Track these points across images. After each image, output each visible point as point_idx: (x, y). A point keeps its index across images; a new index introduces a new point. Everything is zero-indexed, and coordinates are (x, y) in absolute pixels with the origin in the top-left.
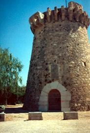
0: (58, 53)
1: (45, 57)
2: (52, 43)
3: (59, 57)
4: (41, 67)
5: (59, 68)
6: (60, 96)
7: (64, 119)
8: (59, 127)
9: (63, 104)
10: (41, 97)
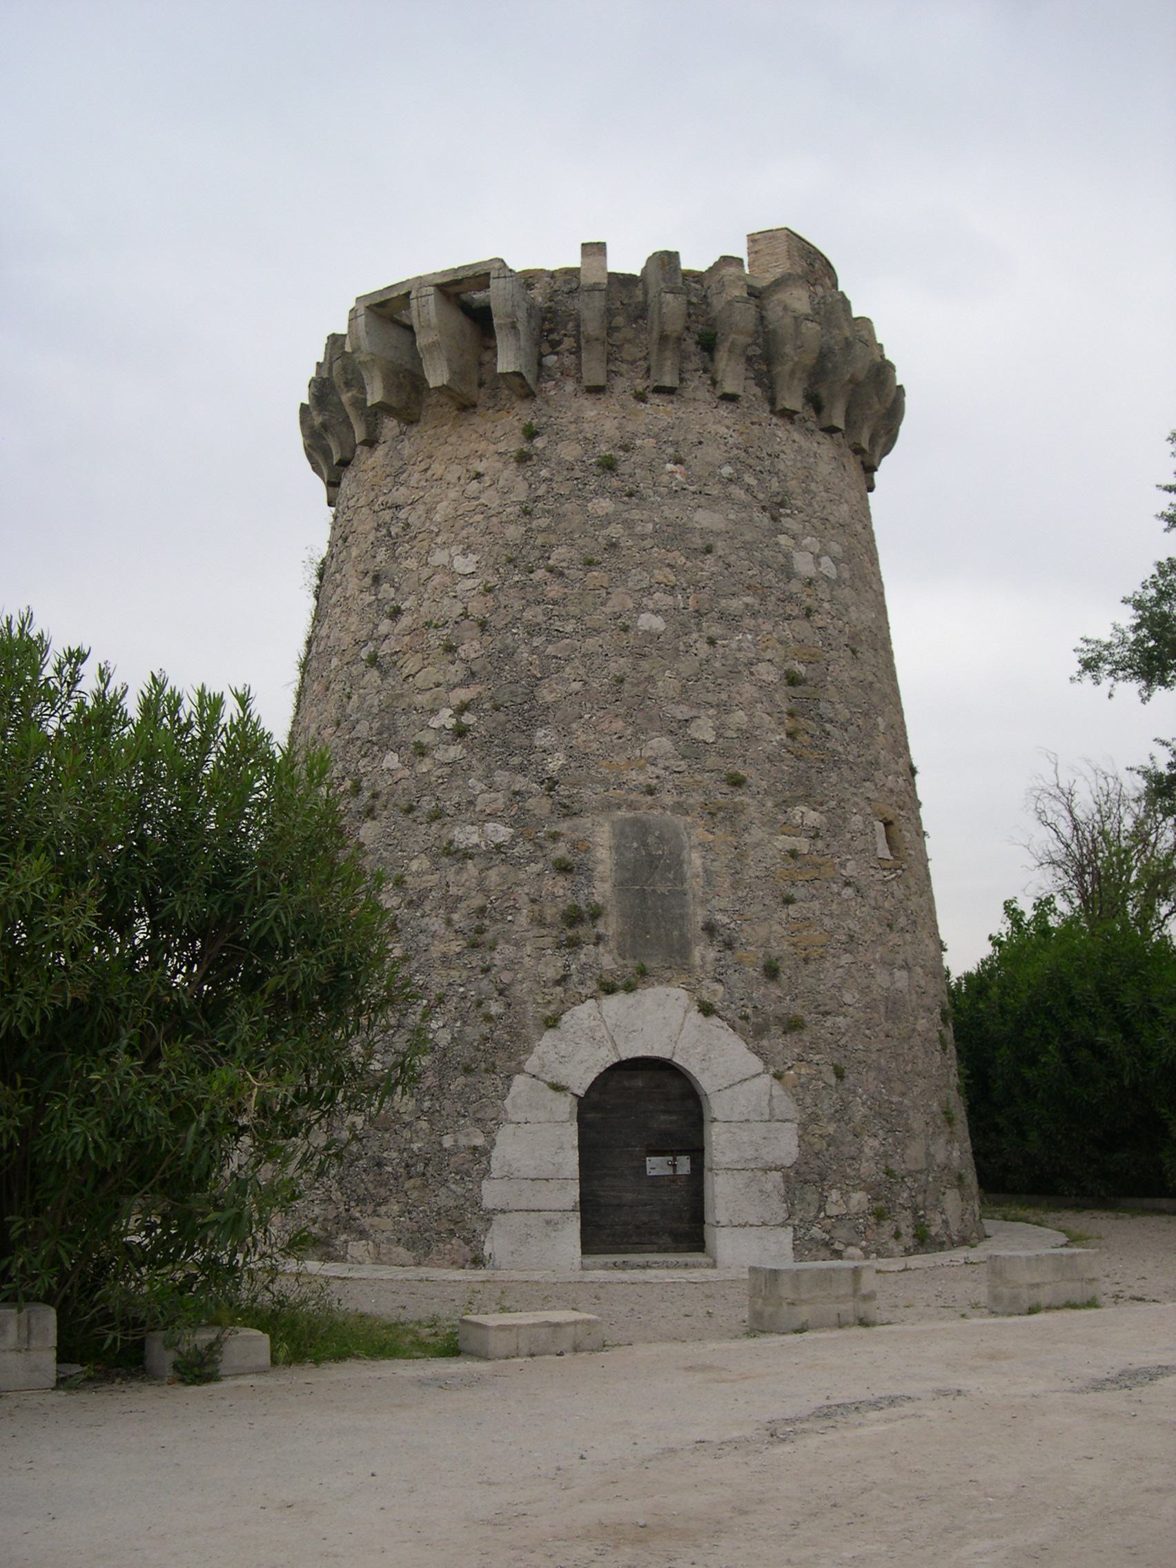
0: (682, 712)
1: (542, 737)
2: (619, 600)
3: (693, 751)
4: (501, 832)
5: (695, 860)
6: (601, 1074)
7: (752, 1333)
8: (1087, 834)
9: (724, 1194)
10: (504, 1136)
